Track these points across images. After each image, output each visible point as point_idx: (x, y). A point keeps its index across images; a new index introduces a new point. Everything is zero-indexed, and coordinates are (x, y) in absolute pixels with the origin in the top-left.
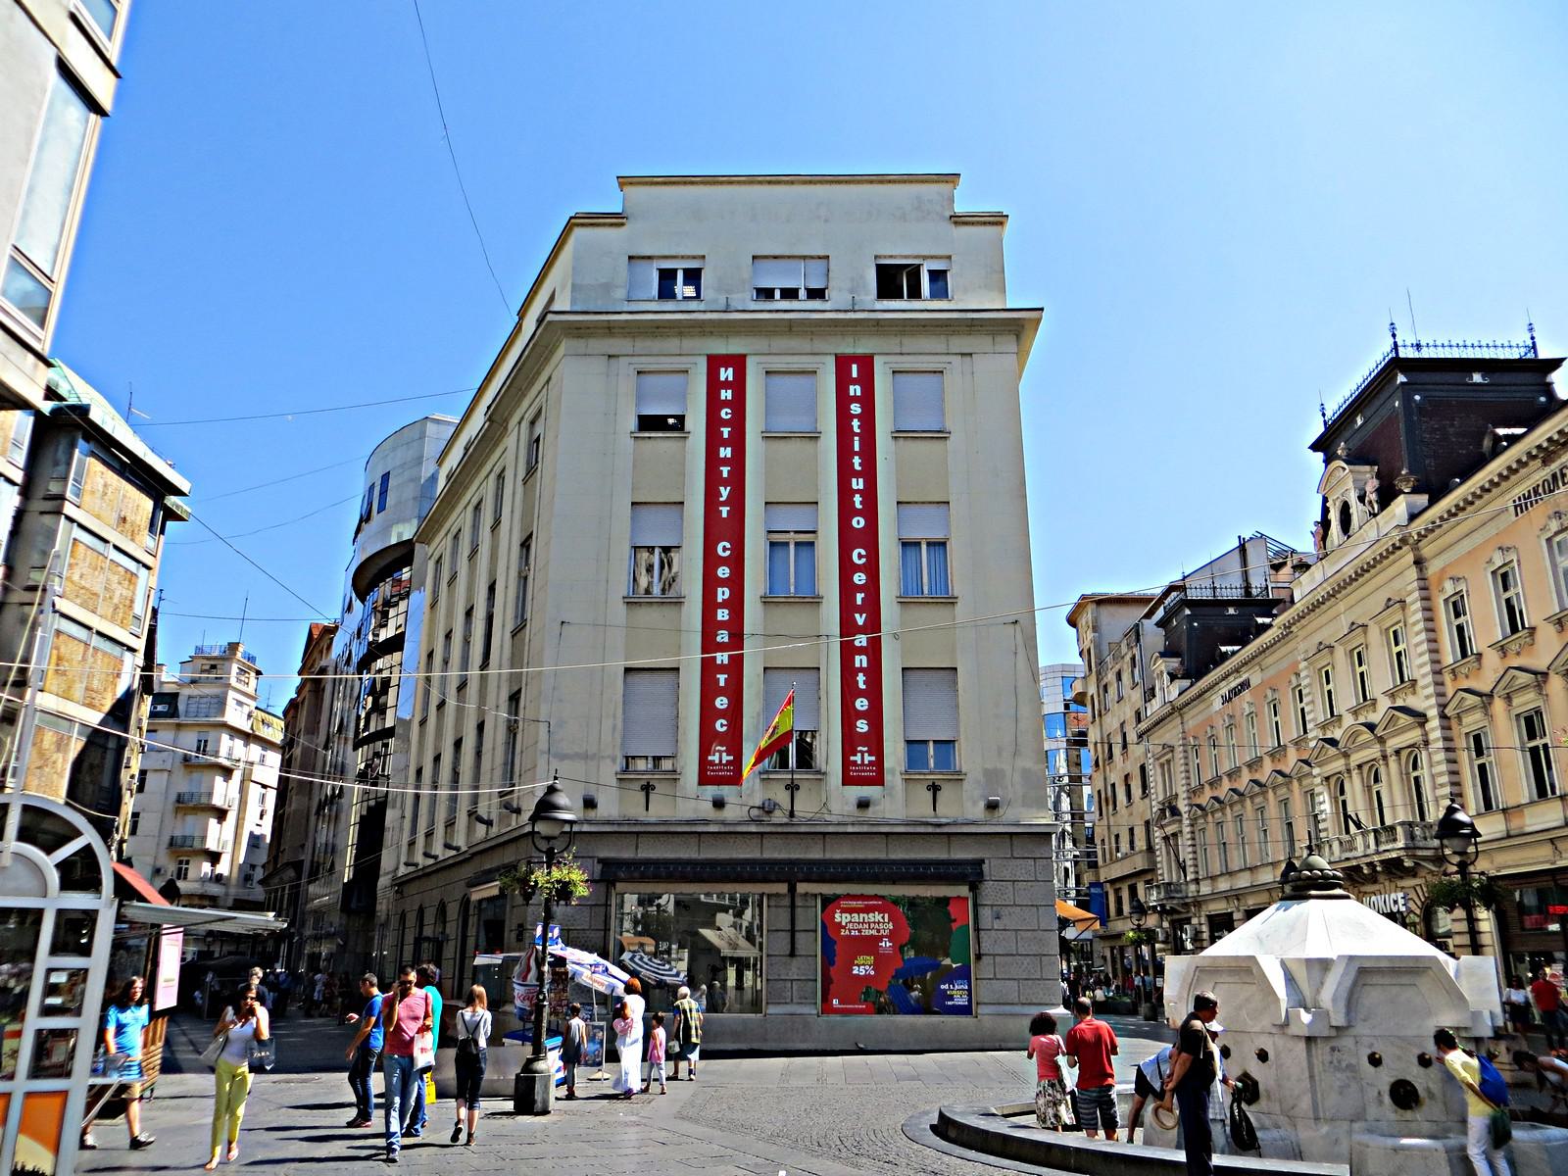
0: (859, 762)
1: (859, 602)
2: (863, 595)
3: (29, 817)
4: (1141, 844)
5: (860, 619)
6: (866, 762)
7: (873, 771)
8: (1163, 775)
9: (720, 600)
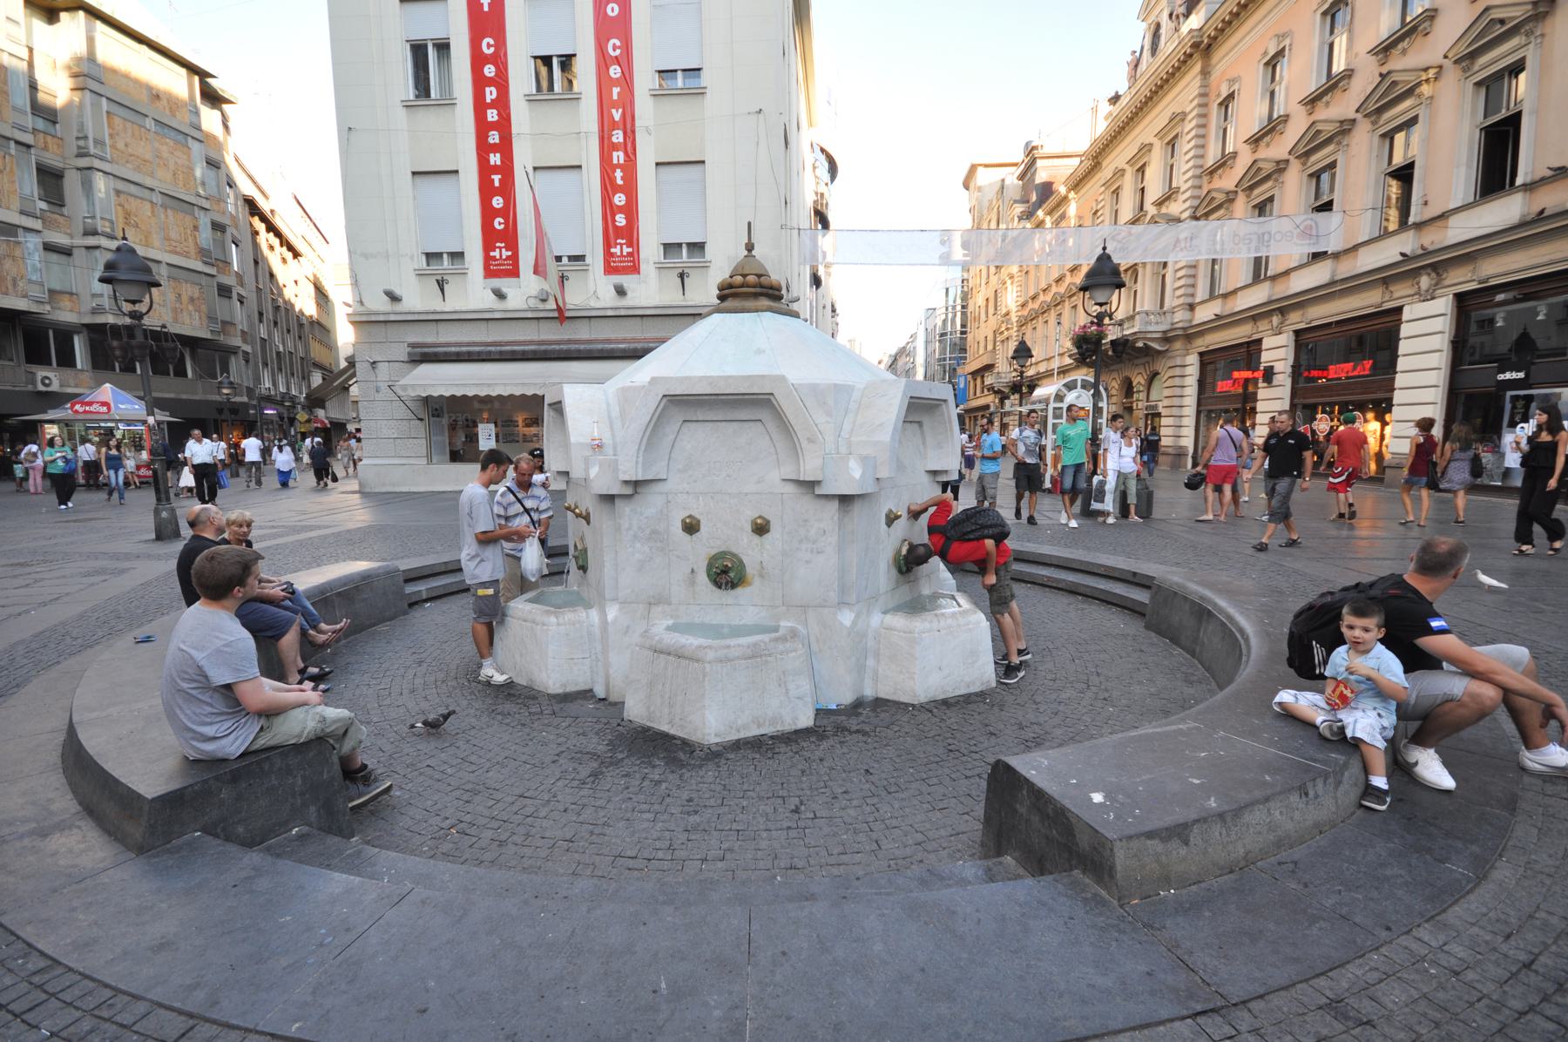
0: (498, 257)
1: (615, 97)
2: (618, 89)
4: (990, 347)
5: (617, 115)
6: (625, 254)
9: (488, 100)
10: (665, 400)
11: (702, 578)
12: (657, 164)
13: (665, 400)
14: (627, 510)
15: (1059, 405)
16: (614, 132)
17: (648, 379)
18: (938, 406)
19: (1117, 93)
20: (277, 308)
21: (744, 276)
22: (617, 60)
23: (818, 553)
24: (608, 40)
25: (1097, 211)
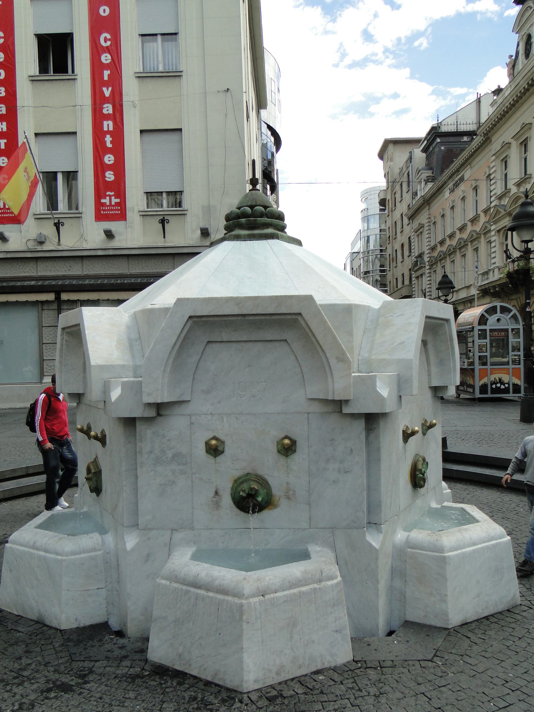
0: (108, 204)
1: (106, 78)
2: (109, 72)
3: (481, 338)
4: (407, 282)
5: (107, 92)
6: (113, 203)
7: (118, 210)
8: (418, 242)
10: (190, 322)
11: (227, 500)
12: (142, 131)
13: (190, 322)
14: (149, 432)
15: (483, 327)
16: (105, 106)
17: (174, 301)
18: (441, 325)
19: (499, 86)
20: (104, 644)
21: (252, 207)
22: (107, 50)
23: (346, 472)
24: (101, 34)
25: (490, 175)
